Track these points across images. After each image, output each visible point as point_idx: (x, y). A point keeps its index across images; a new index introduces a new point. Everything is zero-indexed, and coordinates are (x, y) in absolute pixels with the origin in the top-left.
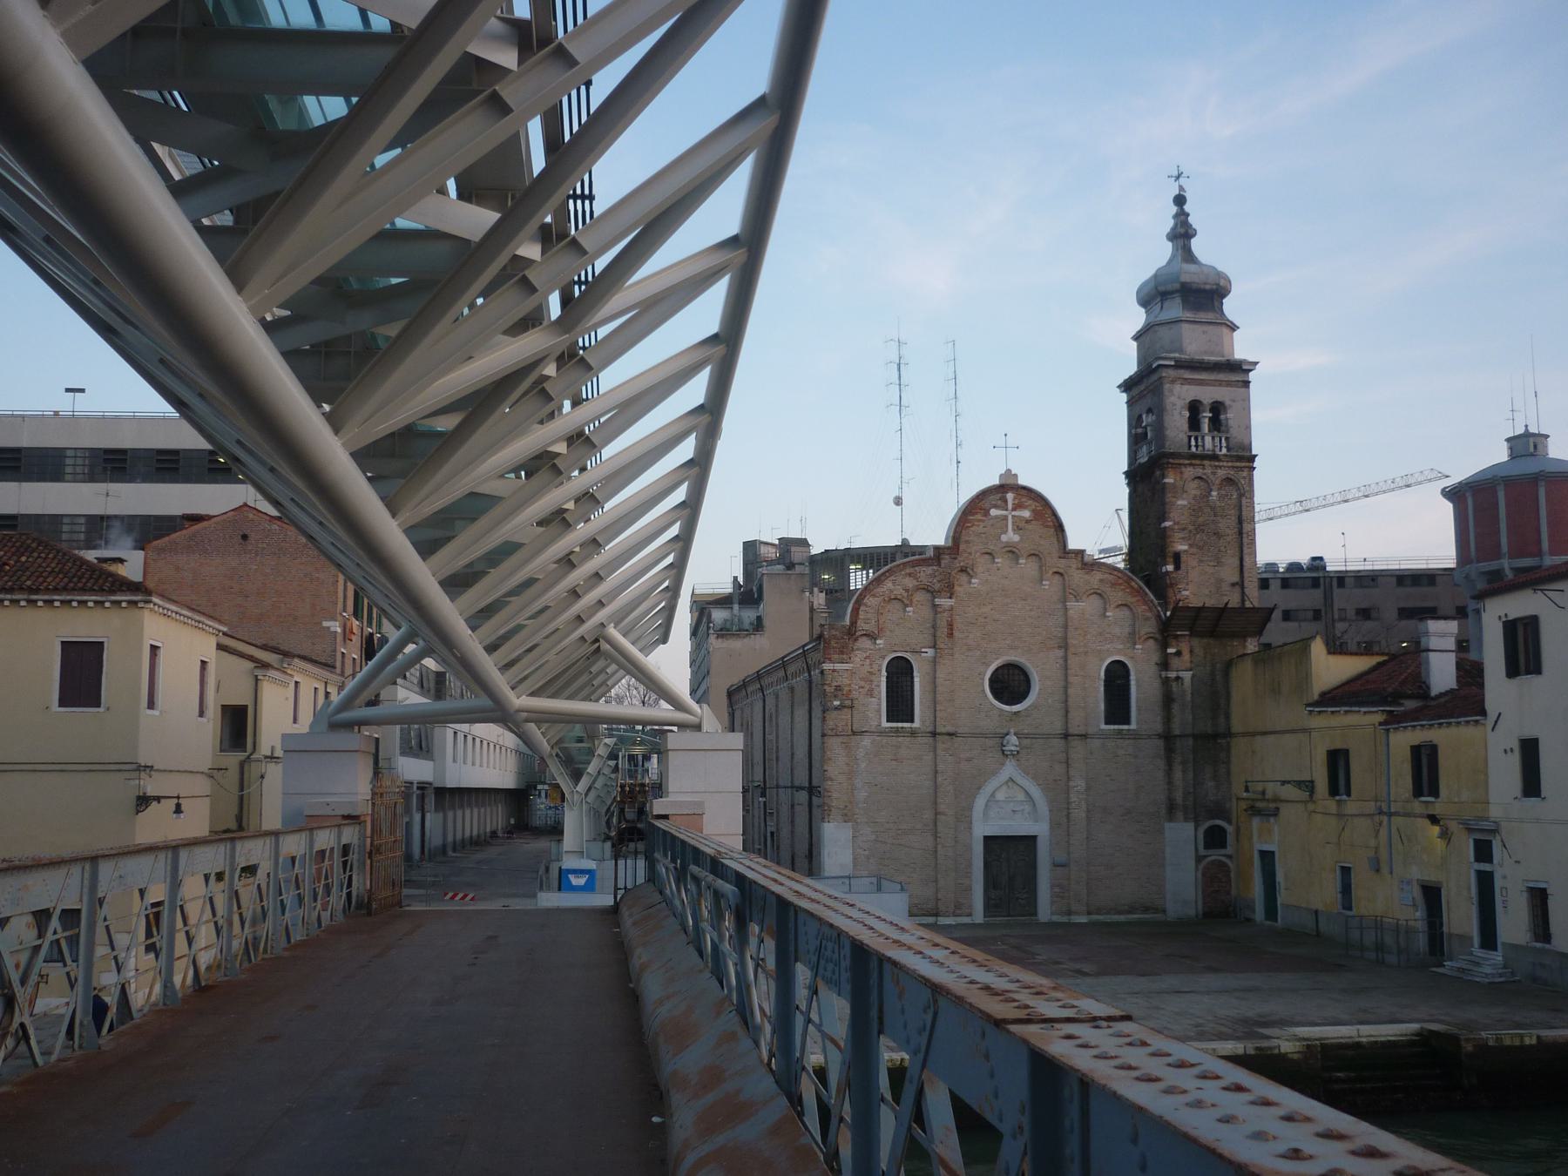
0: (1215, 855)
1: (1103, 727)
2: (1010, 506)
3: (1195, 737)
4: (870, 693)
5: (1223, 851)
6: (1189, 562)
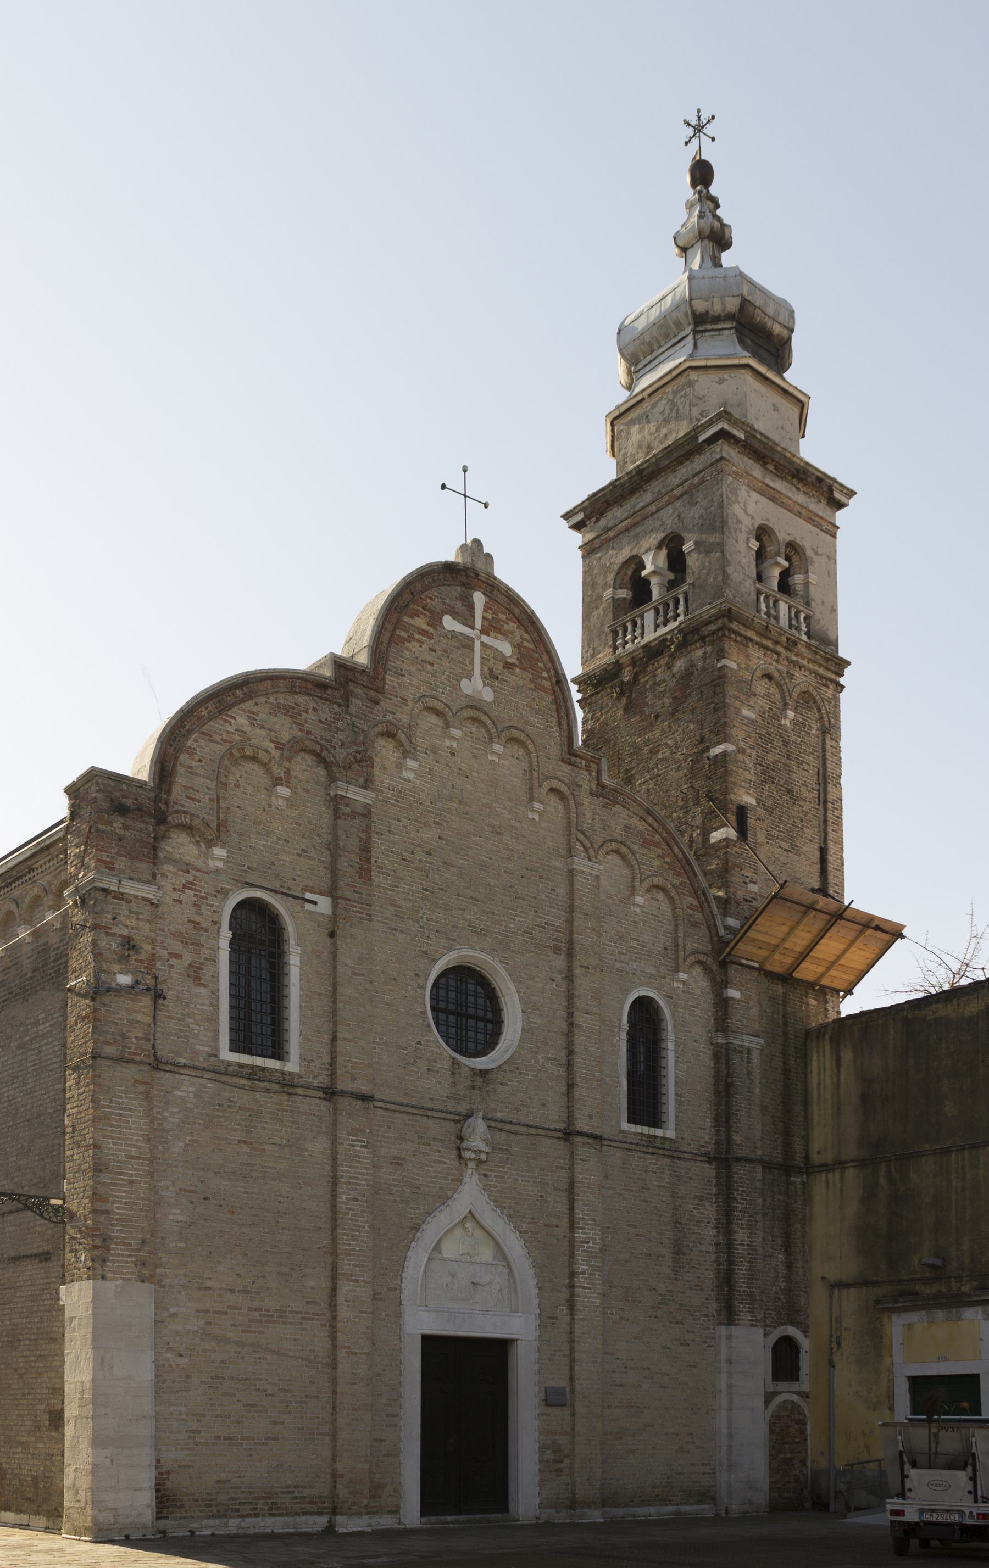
0: (787, 1393)
1: (626, 1126)
2: (478, 623)
4: (196, 973)
5: (795, 1386)
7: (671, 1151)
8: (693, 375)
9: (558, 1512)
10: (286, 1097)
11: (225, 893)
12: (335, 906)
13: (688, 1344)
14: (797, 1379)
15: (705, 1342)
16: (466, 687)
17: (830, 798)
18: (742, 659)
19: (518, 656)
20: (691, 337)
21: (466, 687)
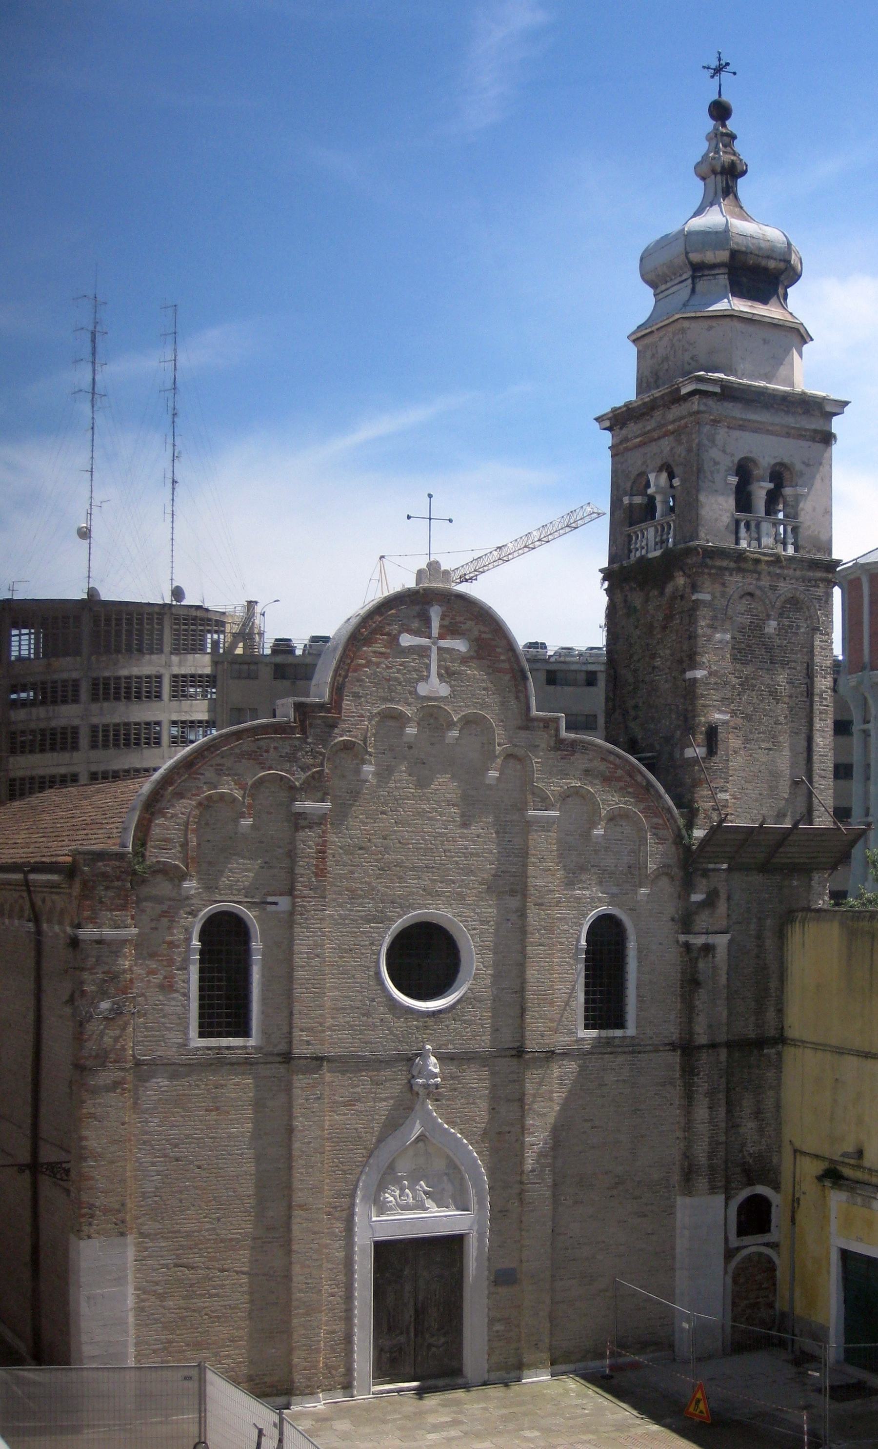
0: (753, 1245)
2: (435, 631)
3: (729, 1045)
4: (168, 987)
6: (731, 741)
7: (633, 1048)
8: (686, 324)
9: (508, 1373)
10: (249, 1067)
11: (193, 914)
12: (294, 905)
13: (645, 1216)
14: (769, 1231)
15: (665, 1211)
16: (423, 689)
17: (817, 691)
18: (718, 588)
19: (476, 648)
20: (690, 281)
21: (423, 689)
